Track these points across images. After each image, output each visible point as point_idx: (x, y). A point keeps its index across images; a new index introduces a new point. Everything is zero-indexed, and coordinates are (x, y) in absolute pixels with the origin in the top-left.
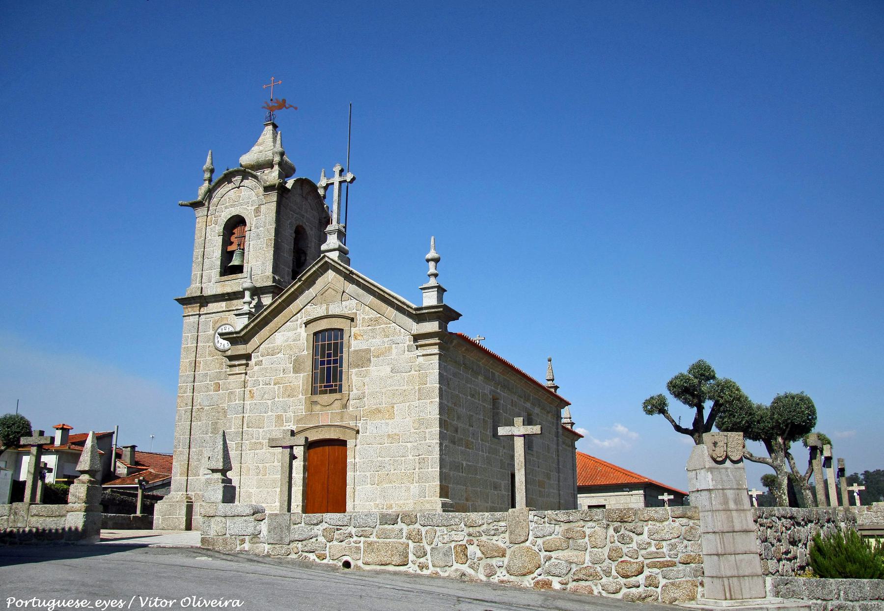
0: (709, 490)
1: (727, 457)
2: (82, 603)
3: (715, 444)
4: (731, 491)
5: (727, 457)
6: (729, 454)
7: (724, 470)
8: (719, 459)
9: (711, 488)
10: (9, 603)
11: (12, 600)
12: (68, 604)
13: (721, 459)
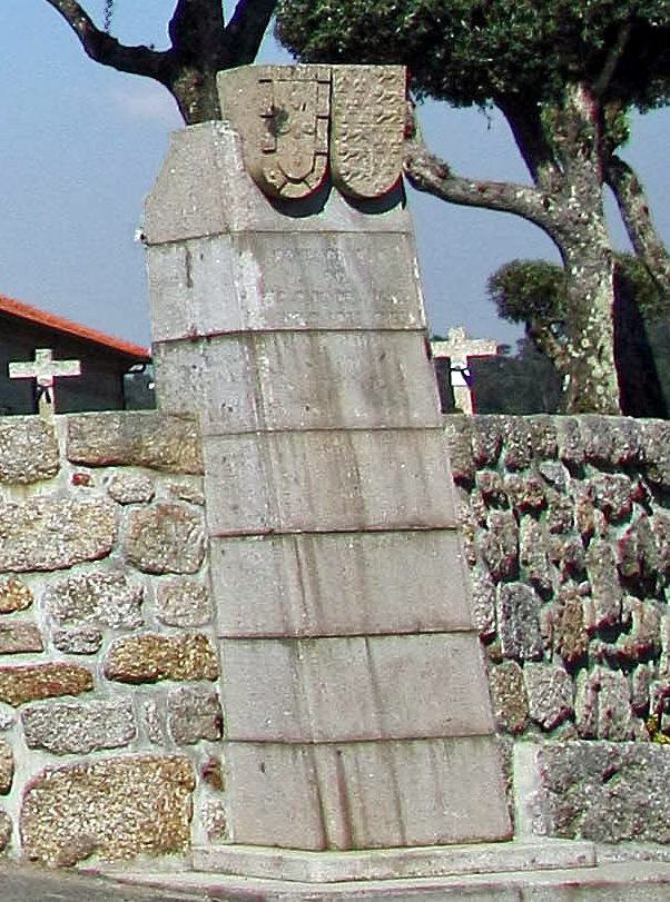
0: (248, 336)
1: (331, 180)
4: (353, 342)
5: (331, 180)
7: (315, 244)
13: (300, 191)
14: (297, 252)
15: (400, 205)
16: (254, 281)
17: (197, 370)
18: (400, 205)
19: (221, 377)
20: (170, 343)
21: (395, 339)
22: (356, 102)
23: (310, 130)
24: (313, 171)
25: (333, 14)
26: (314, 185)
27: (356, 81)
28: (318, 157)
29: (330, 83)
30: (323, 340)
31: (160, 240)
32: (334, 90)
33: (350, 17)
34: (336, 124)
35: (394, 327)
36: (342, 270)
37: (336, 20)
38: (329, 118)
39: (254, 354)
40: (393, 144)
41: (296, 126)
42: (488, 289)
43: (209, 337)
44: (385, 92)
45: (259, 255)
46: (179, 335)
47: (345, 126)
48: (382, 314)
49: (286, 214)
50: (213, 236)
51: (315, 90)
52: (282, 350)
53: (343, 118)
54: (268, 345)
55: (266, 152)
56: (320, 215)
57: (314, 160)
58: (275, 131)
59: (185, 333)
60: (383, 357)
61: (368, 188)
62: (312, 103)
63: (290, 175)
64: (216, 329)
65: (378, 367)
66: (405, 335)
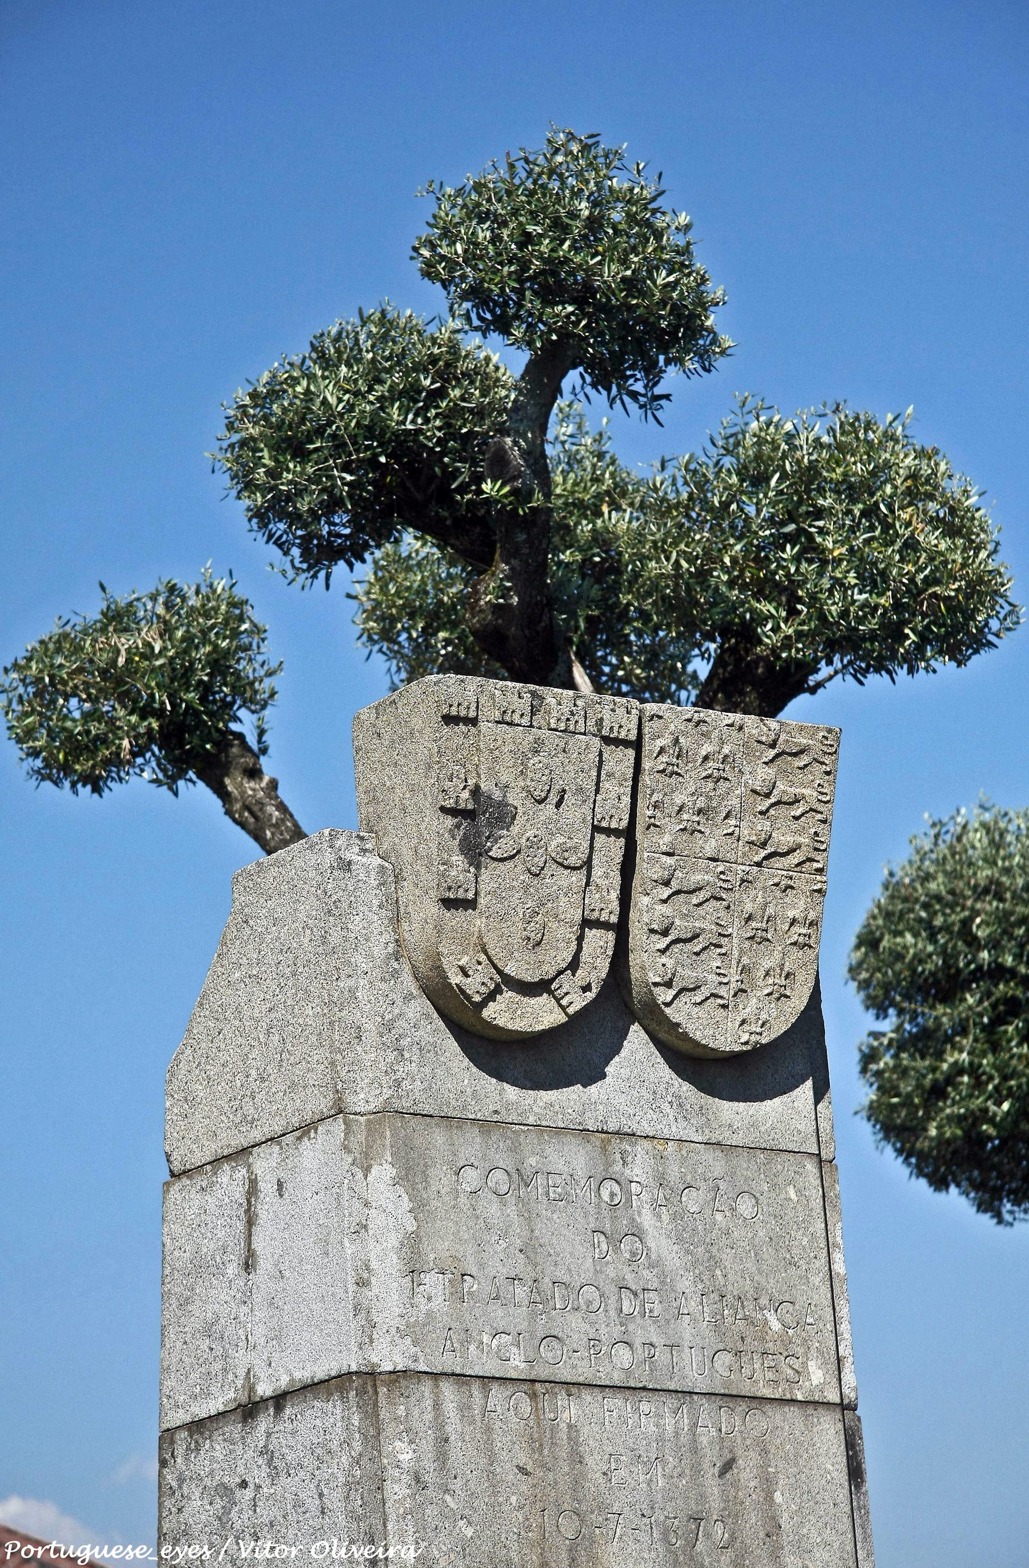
0: (362, 1384)
1: (619, 1004)
2: (137, 1551)
3: (477, 820)
4: (652, 1421)
5: (619, 1004)
6: (648, 963)
7: (574, 1159)
8: (509, 1014)
9: (389, 1355)
10: (9, 1551)
11: (14, 1546)
12: (113, 1553)
13: (541, 1015)
14: (521, 1178)
15: (807, 1088)
16: (393, 1240)
17: (249, 1493)
18: (807, 1088)
19: (298, 1504)
20: (197, 1427)
21: (759, 1422)
22: (701, 803)
23: (573, 861)
24: (574, 965)
25: (973, 1070)
26: (577, 1002)
27: (706, 749)
28: (590, 934)
29: (637, 745)
30: (570, 1410)
31: (198, 1158)
32: (647, 764)
33: (1005, 1078)
34: (642, 856)
35: (767, 1392)
36: (638, 1234)
37: (978, 1084)
38: (629, 834)
39: (374, 1435)
40: (794, 922)
41: (534, 844)
42: (881, 1136)
43: (280, 1400)
44: (781, 786)
45: (411, 1174)
46: (215, 1405)
47: (670, 861)
48: (738, 1353)
49: (500, 1078)
50: (306, 1129)
51: (593, 757)
52: (453, 1426)
53: (665, 840)
54: (417, 1406)
55: (449, 904)
56: (593, 1089)
57: (580, 939)
58: (475, 853)
59: (232, 1395)
60: (728, 1466)
61: (723, 1033)
62: (580, 790)
63: (510, 970)
64: (298, 1375)
65: (713, 1487)
66: (792, 1412)
